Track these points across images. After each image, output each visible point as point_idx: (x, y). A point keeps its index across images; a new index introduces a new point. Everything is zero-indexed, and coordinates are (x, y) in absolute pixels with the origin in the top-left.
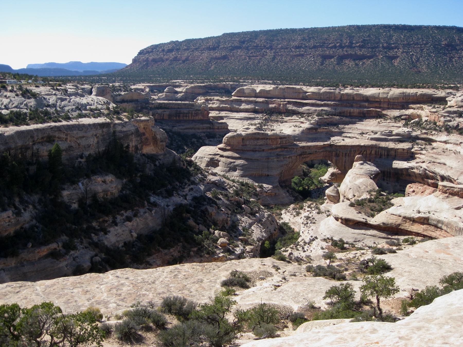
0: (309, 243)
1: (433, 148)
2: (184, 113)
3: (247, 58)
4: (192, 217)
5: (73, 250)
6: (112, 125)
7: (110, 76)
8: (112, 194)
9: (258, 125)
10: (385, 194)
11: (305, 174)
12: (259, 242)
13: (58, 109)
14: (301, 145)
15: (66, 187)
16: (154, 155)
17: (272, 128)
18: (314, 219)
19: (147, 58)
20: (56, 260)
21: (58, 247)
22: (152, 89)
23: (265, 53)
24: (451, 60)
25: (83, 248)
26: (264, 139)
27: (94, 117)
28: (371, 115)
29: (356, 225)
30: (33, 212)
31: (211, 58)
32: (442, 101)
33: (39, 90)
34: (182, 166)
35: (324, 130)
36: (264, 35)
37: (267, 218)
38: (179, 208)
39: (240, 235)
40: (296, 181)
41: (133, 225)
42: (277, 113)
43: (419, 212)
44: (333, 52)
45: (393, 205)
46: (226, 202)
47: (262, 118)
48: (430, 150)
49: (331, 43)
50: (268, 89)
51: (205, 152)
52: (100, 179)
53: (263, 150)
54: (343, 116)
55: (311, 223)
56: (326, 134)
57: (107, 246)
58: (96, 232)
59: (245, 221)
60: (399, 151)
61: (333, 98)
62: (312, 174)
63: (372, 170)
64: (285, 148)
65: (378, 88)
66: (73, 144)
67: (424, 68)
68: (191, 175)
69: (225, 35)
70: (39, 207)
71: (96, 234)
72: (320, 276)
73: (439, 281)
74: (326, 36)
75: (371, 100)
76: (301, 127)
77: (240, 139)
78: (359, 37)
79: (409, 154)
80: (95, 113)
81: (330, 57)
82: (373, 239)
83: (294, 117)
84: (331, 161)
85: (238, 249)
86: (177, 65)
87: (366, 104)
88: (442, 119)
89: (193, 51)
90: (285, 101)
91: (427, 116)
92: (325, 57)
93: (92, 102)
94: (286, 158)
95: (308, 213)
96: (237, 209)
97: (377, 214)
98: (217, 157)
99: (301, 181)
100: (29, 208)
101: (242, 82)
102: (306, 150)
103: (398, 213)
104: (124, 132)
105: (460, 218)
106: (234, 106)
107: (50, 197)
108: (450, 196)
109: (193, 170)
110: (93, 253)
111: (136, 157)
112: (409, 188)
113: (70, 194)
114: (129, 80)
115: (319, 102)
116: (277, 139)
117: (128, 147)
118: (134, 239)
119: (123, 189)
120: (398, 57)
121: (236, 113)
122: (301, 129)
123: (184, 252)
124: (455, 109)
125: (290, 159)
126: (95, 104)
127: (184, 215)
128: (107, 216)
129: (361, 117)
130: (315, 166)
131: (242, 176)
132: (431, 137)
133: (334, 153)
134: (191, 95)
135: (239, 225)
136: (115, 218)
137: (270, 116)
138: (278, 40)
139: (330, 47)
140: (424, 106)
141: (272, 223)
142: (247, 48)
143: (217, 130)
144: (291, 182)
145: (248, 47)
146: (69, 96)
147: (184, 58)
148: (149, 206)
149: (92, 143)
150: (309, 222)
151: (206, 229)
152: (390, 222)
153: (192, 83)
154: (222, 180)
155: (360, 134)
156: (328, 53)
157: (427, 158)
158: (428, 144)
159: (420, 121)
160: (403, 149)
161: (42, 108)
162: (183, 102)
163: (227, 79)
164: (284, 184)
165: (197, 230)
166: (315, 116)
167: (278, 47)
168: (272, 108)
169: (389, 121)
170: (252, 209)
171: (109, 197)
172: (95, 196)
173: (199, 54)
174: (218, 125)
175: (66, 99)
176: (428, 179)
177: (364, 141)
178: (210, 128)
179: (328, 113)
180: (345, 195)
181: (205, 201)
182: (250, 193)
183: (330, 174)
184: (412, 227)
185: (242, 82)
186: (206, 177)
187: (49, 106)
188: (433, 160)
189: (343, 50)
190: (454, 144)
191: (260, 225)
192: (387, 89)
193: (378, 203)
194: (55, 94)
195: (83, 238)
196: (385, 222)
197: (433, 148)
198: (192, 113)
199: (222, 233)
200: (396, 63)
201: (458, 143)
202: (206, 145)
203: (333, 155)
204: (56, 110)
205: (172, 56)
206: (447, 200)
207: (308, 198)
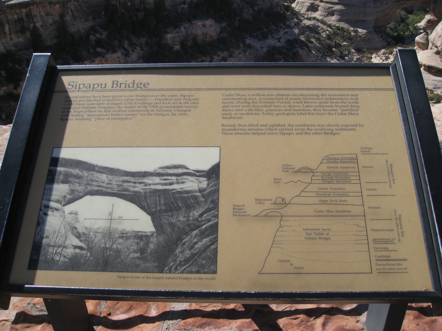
11: (403, 20)
30: (140, 53)
40: (392, 27)
46: (318, 45)
52: (200, 23)
62: (409, 21)
68: (288, 20)
70: (145, 49)
84: (429, 8)
96: (327, 52)
99: (396, 27)
100: (136, 49)
109: (290, 15)
113: (173, 37)
119: (221, 32)
127: (276, 56)
130: (414, 12)
131: (339, 21)
154: (316, 24)
164: (378, 29)
170: (341, 53)
172: (195, 38)
180: (434, 42)
182: (344, 37)
183: (426, 21)
186: (301, 22)
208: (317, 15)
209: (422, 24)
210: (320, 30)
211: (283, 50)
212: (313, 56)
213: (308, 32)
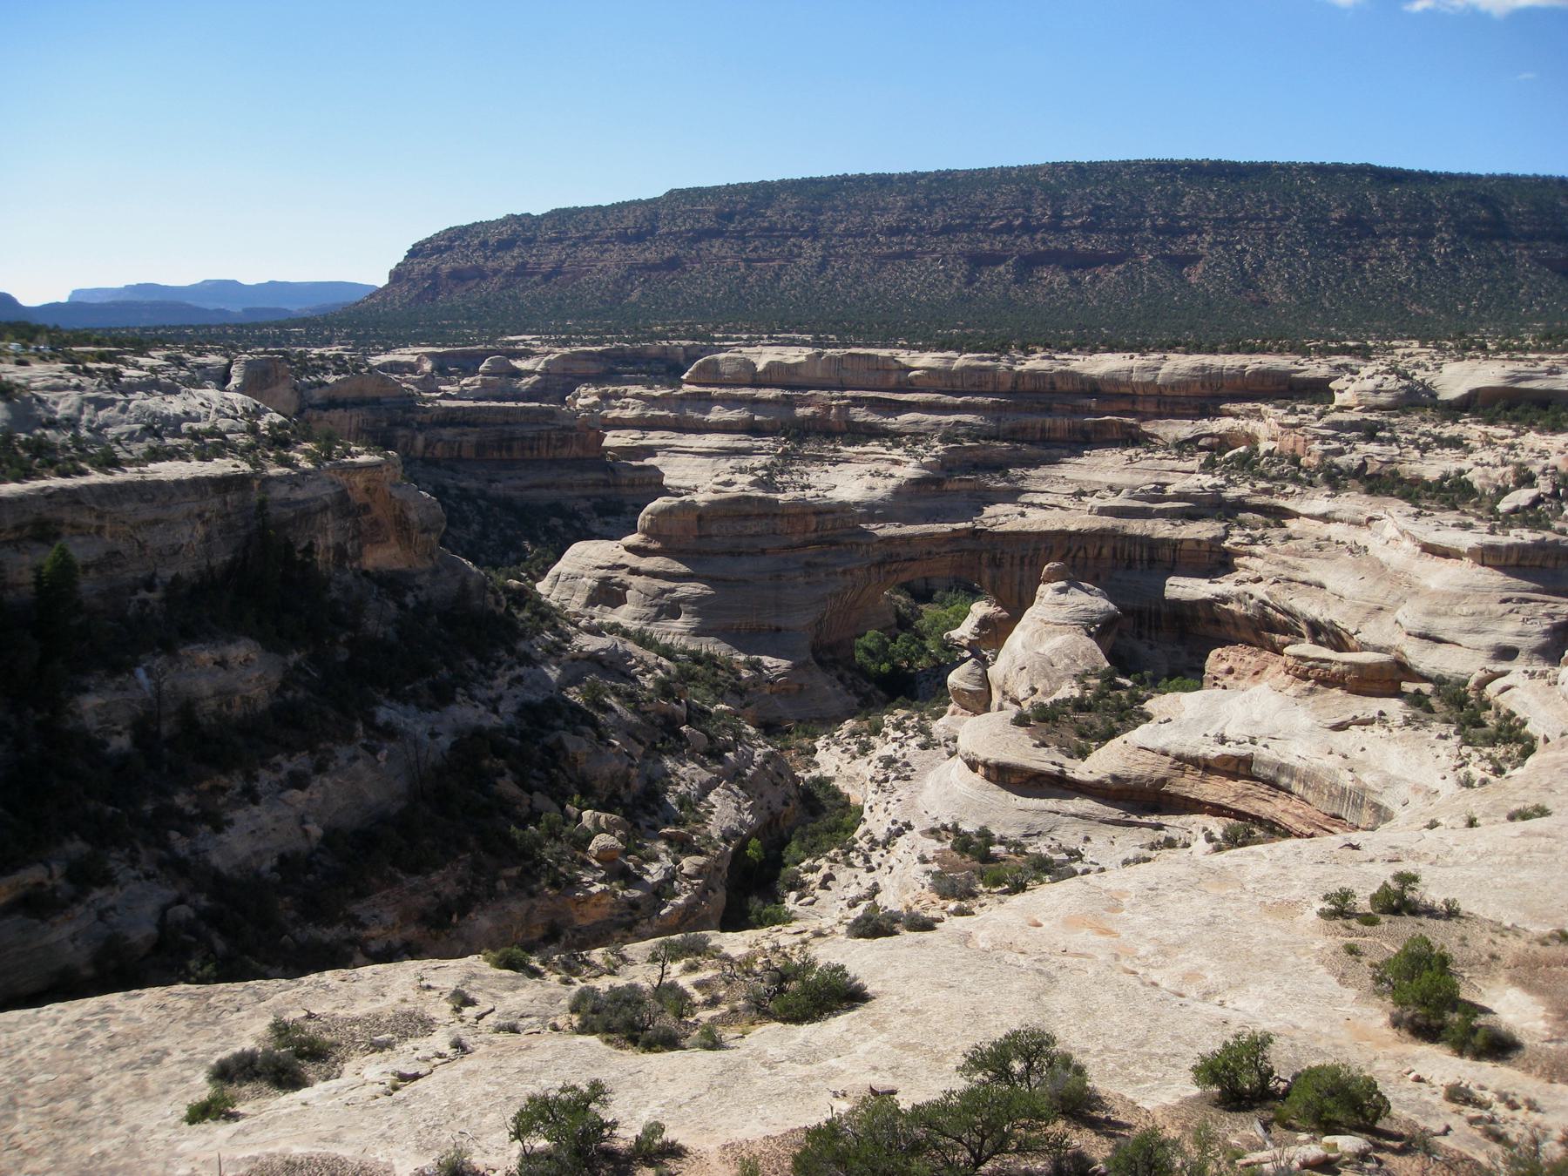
0: (887, 843)
1: (1289, 537)
2: (524, 438)
3: (742, 264)
4: (510, 768)
5: (101, 885)
6: (256, 483)
7: (318, 325)
8: (246, 700)
9: (760, 473)
10: (1129, 683)
11: (904, 622)
12: (727, 841)
13: (84, 433)
14: (881, 533)
15: (91, 681)
16: (400, 573)
17: (805, 481)
18: (907, 764)
19: (436, 268)
20: (36, 921)
21: (51, 876)
22: (443, 366)
23: (796, 250)
24: (1357, 267)
25: (138, 878)
26: (766, 515)
27: (202, 458)
31: (631, 266)
32: (1319, 391)
33: (25, 374)
34: (492, 606)
35: (963, 485)
36: (794, 195)
37: (762, 766)
38: (472, 744)
39: (667, 823)
40: (871, 645)
41: (310, 800)
42: (818, 433)
44: (1004, 243)
46: (629, 717)
47: (775, 449)
48: (1277, 544)
49: (998, 218)
50: (793, 361)
51: (584, 561)
52: (206, 655)
53: (763, 551)
54: (1023, 442)
55: (897, 778)
56: (970, 496)
57: (217, 871)
58: (186, 824)
59: (687, 774)
60: (1184, 546)
61: (990, 387)
62: (923, 623)
63: (1095, 607)
64: (832, 543)
66: (122, 546)
67: (1277, 293)
69: (674, 196)
71: (185, 833)
72: (593, 1032)
73: (962, 1061)
74: (980, 196)
75: (1107, 389)
76: (891, 476)
77: (692, 518)
78: (1081, 199)
79: (1214, 557)
80: (207, 445)
81: (995, 259)
82: (1081, 828)
83: (873, 446)
85: (653, 868)
86: (523, 290)
87: (1093, 403)
88: (1317, 447)
89: (574, 245)
90: (844, 398)
91: (1274, 439)
92: (978, 261)
93: (203, 410)
95: (895, 745)
96: (663, 740)
97: (1098, 747)
98: (621, 575)
99: (885, 645)
101: (719, 340)
102: (899, 549)
103: (1160, 743)
104: (298, 502)
105: (1345, 757)
106: (689, 413)
107: (38, 717)
108: (1319, 687)
110: (171, 893)
111: (339, 583)
112: (1215, 662)
113: (104, 706)
114: (373, 337)
115: (948, 399)
116: (806, 514)
117: (309, 550)
118: (315, 844)
119: (284, 686)
120: (1199, 258)
121: (693, 436)
122: (892, 482)
123: (476, 882)
124: (1354, 416)
125: (849, 577)
126: (212, 416)
127: (486, 762)
128: (225, 771)
129: (1075, 442)
131: (698, 632)
132: (1281, 502)
133: (985, 555)
134: (559, 382)
135: (666, 791)
136: (251, 777)
137: (800, 444)
138: (835, 209)
139: (993, 231)
140: (1263, 407)
141: (778, 780)
142: (741, 236)
144: (852, 648)
145: (745, 230)
146: (123, 393)
147: (546, 268)
148: (369, 737)
149: (184, 542)
150: (893, 775)
151: (555, 806)
152: (1136, 771)
153: (565, 343)
155: (1074, 495)
156: (986, 246)
157: (1268, 567)
158: (1272, 522)
159: (1251, 454)
160: (1198, 542)
161: (29, 432)
162: (521, 404)
163: (672, 331)
164: (829, 655)
165: (523, 810)
167: (836, 231)
168: (805, 419)
169: (1160, 454)
170: (711, 739)
171: (237, 711)
172: (187, 709)
173: (595, 255)
174: (630, 475)
175: (113, 402)
176: (1264, 630)
177: (1079, 519)
178: (607, 484)
179: (974, 433)
181: (559, 716)
183: (976, 622)
184: (1203, 786)
185: (719, 340)
186: (569, 641)
187: (52, 424)
188: (1286, 574)
189: (1032, 240)
190: (1351, 523)
191: (735, 788)
192: (1155, 356)
193: (1104, 711)
194: (78, 387)
195: (139, 845)
196: (1119, 771)
197: (1289, 537)
198: (549, 438)
199: (603, 816)
200: (1194, 275)
201: (1363, 518)
202: (590, 536)
203: (984, 562)
204: (76, 439)
205: (509, 260)
206: (1311, 699)
207: (899, 699)
208: (623, 615)
209: (965, 631)
213: (594, 676)
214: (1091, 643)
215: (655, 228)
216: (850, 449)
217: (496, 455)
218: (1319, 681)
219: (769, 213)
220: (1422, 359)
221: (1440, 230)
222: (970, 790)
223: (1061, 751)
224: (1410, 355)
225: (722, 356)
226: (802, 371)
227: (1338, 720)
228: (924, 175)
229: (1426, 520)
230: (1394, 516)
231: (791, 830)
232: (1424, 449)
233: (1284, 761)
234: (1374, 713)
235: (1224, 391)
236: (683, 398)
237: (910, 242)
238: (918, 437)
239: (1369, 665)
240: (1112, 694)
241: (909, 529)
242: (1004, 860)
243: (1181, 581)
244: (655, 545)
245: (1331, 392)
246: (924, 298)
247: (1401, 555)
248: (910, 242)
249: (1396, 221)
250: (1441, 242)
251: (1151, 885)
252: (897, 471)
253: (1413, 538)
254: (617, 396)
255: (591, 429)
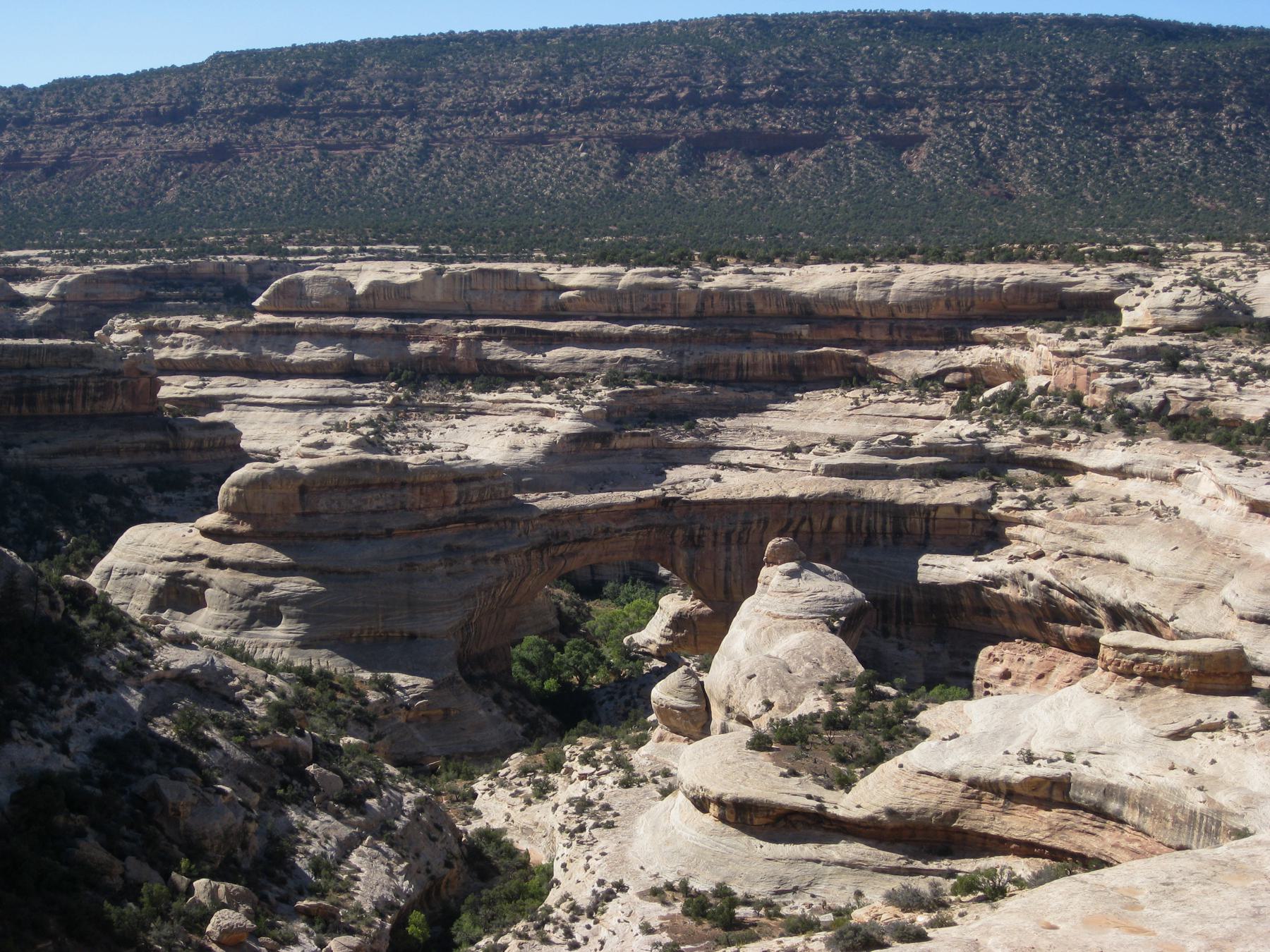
0: (593, 911)
1: (1075, 499)
3: (315, 152)
4: (93, 826)
9: (365, 430)
10: (893, 692)
11: (568, 626)
12: (382, 916)
17: (425, 440)
18: (607, 807)
24: (1126, 150)
26: (391, 485)
28: (825, 374)
29: (782, 823)
34: (45, 609)
35: (637, 441)
36: (383, 60)
37: (415, 816)
39: (301, 894)
40: (530, 655)
42: (440, 376)
43: (1030, 758)
44: (666, 122)
45: (924, 734)
46: (239, 755)
47: (383, 398)
48: (1060, 508)
49: (657, 88)
50: (403, 280)
51: (144, 550)
53: (389, 533)
54: (713, 382)
55: (596, 826)
56: (645, 455)
59: (319, 830)
60: (940, 514)
61: (669, 311)
63: (837, 595)
65: (848, 266)
67: (1026, 183)
68: (88, 649)
69: (219, 60)
74: (632, 60)
75: (823, 311)
76: (541, 431)
78: (766, 63)
79: (980, 526)
81: (654, 143)
82: (849, 881)
83: (515, 392)
84: (671, 566)
86: (17, 189)
87: (804, 331)
88: (1103, 381)
89: (87, 127)
90: (473, 328)
91: (1046, 372)
92: (632, 146)
94: (485, 560)
95: (585, 784)
96: (284, 785)
97: (864, 774)
98: (197, 569)
99: (549, 656)
101: (294, 253)
102: (567, 527)
103: (947, 765)
105: (1192, 772)
108: (1148, 686)
109: (94, 627)
112: (988, 663)
115: (612, 328)
116: (444, 483)
120: (921, 139)
121: (271, 382)
122: (543, 440)
124: (1149, 340)
125: (503, 564)
127: (61, 819)
129: (784, 382)
131: (305, 643)
132: (1062, 454)
134: (80, 311)
135: (295, 852)
137: (416, 390)
138: (439, 78)
139: (650, 106)
140: (1030, 332)
141: (435, 834)
143: (195, 456)
144: (509, 660)
145: (318, 107)
147: (48, 159)
150: (590, 823)
151: (155, 875)
152: (917, 803)
153: (85, 260)
154: (218, 664)
155: (784, 451)
156: (642, 126)
157: (1052, 538)
159: (1018, 392)
160: (958, 508)
162: (46, 342)
163: (229, 242)
164: (479, 669)
166: (597, 385)
168: (422, 357)
169: (895, 396)
170: (347, 782)
173: (115, 140)
174: (197, 435)
176: (1060, 623)
177: (799, 482)
178: (165, 448)
179: (649, 372)
180: (732, 703)
183: (667, 621)
184: (1006, 818)
185: (294, 253)
186: (150, 656)
188: (1076, 545)
189: (703, 117)
191: (383, 845)
192: (884, 267)
193: (864, 729)
196: (896, 804)
197: (1075, 499)
198: (86, 387)
199: (222, 887)
200: (917, 161)
201: (1170, 471)
202: (147, 518)
203: (678, 540)
207: (581, 724)
208: (199, 623)
209: (653, 633)
210: (238, 688)
211: (88, 788)
212: (228, 804)
213: (186, 701)
214: (836, 640)
215: (196, 105)
216: (484, 396)
217: (13, 410)
218: (1147, 677)
219: (350, 84)
220: (1229, 265)
221: (1229, 101)
222: (701, 836)
223: (816, 781)
224: (1212, 261)
225: (307, 275)
226: (416, 293)
227: (1178, 726)
228: (557, 33)
229: (1253, 471)
230: (1211, 467)
231: (460, 900)
232: (1242, 380)
233: (1113, 781)
234: (1222, 715)
235: (975, 311)
236: (257, 332)
237: (541, 122)
238: (574, 378)
239: (1210, 655)
240: (875, 705)
241: (579, 500)
242: (754, 925)
243: (937, 559)
244: (243, 528)
245: (1116, 311)
246: (561, 196)
247: (1224, 517)
248: (541, 122)
249: (1173, 89)
250: (1232, 115)
251: (1163, 878)
252: (549, 424)
253: (1238, 495)
254: (166, 330)
255: (143, 373)
